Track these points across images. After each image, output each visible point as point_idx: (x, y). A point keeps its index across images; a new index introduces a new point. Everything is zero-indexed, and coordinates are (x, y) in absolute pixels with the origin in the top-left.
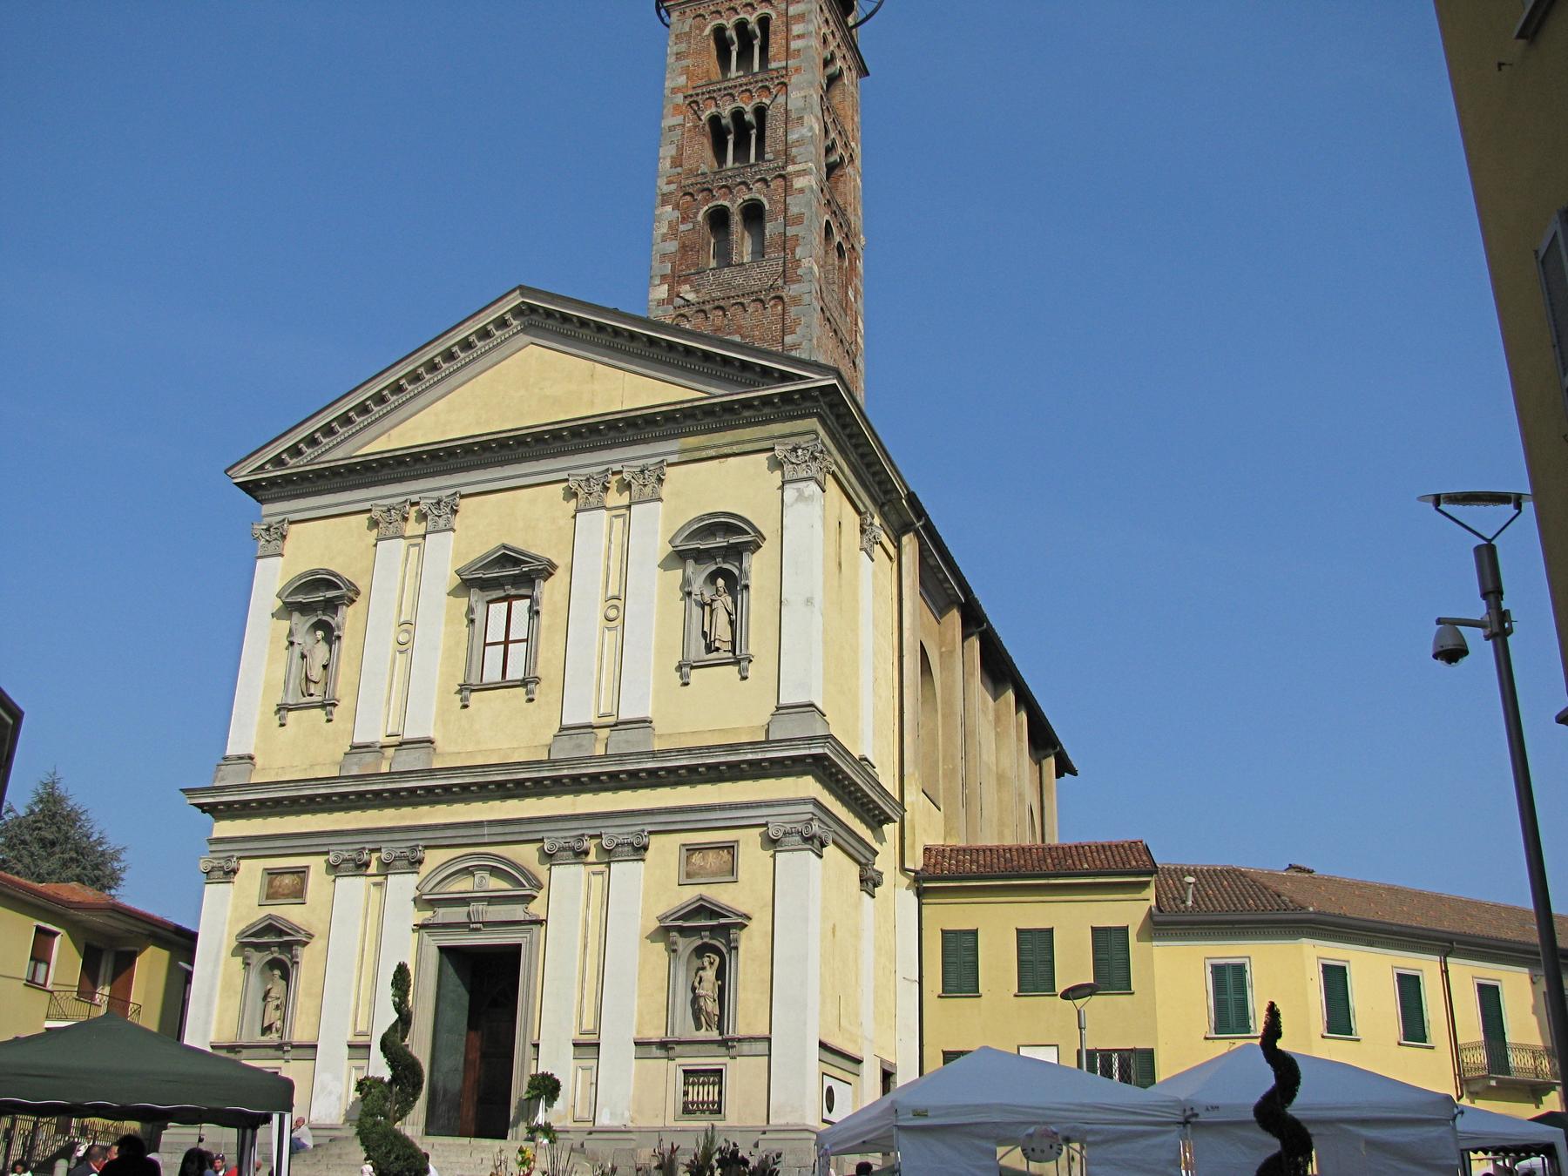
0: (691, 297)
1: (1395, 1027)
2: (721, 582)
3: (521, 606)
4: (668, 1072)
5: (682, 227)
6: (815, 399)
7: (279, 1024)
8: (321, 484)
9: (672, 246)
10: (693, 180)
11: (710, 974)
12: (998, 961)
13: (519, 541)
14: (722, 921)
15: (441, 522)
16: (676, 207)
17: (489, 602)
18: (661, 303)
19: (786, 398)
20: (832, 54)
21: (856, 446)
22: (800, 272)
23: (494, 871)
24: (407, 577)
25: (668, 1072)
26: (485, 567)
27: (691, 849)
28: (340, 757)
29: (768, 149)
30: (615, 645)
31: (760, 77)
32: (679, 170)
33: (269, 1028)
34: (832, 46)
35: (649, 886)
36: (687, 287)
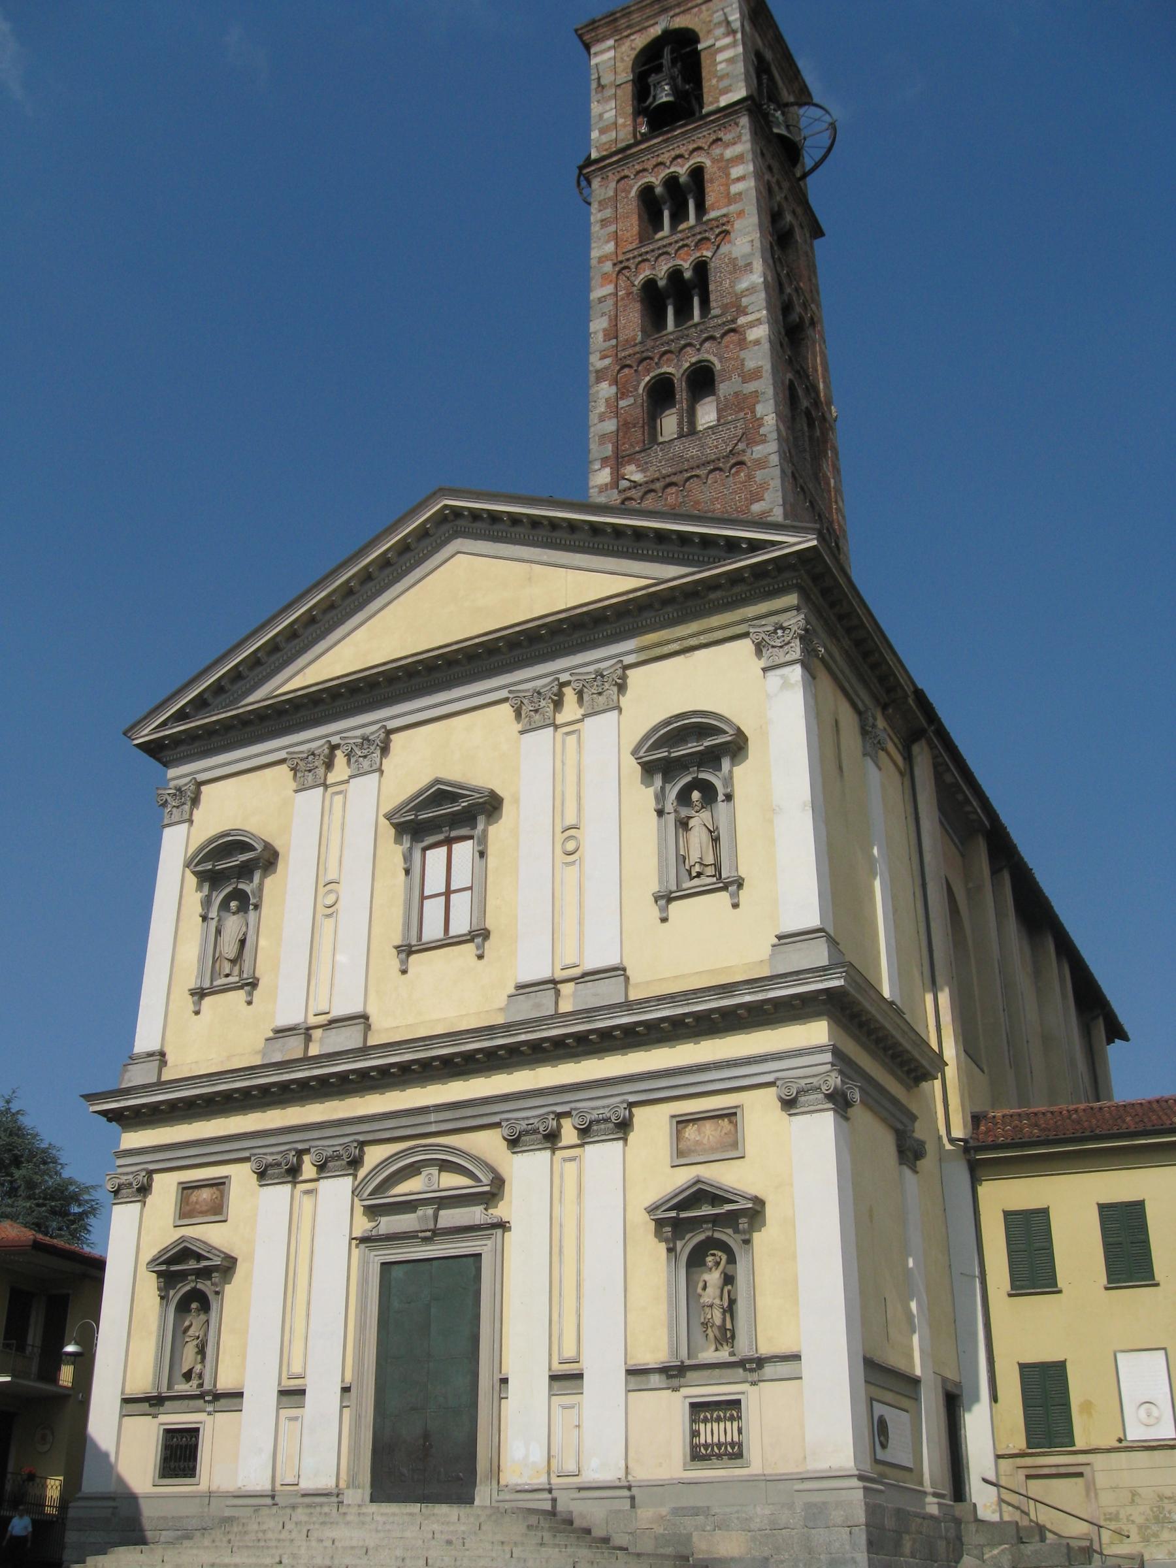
0: (638, 477)
2: (696, 795)
3: (464, 851)
4: (668, 1409)
5: (622, 403)
6: (793, 567)
9: (610, 426)
10: (630, 351)
11: (713, 1278)
13: (456, 772)
16: (615, 382)
17: (425, 849)
18: (603, 489)
19: (758, 571)
20: (780, 205)
21: (849, 631)
22: (762, 431)
23: (445, 1166)
24: (327, 825)
25: (668, 1409)
26: (419, 808)
27: (682, 1122)
28: (261, 1044)
29: (713, 304)
30: (578, 874)
31: (698, 230)
32: (614, 342)
34: (779, 197)
35: (638, 1169)
36: (632, 468)
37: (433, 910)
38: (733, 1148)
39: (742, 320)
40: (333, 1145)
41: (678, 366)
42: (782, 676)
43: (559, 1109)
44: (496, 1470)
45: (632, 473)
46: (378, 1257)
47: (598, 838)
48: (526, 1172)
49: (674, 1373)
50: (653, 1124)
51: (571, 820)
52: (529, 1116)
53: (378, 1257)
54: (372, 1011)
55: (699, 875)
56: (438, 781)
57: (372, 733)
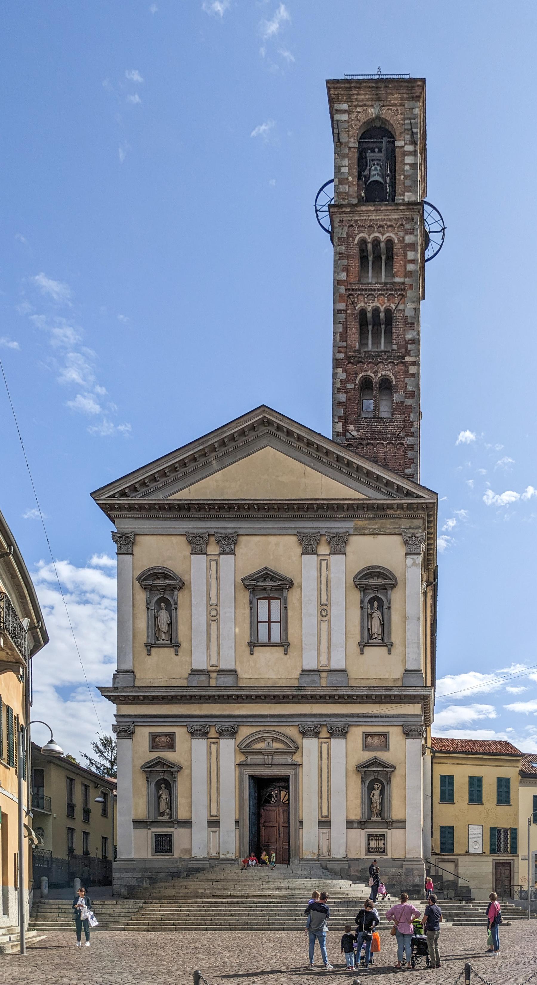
1: (100, 812)
2: (376, 603)
3: (276, 604)
4: (359, 837)
7: (168, 811)
8: (153, 513)
11: (377, 793)
12: (461, 789)
14: (385, 769)
15: (338, 548)
17: (258, 599)
23: (275, 739)
25: (359, 837)
33: (163, 812)
35: (348, 752)
37: (263, 629)
38: (386, 747)
39: (407, 359)
40: (227, 725)
41: (376, 373)
42: (413, 559)
43: (322, 723)
44: (298, 853)
45: (352, 430)
46: (247, 772)
47: (337, 610)
48: (309, 745)
49: (362, 824)
50: (356, 734)
51: (324, 601)
52: (310, 723)
53: (247, 772)
54: (239, 670)
55: (376, 638)
56: (266, 569)
57: (231, 534)
